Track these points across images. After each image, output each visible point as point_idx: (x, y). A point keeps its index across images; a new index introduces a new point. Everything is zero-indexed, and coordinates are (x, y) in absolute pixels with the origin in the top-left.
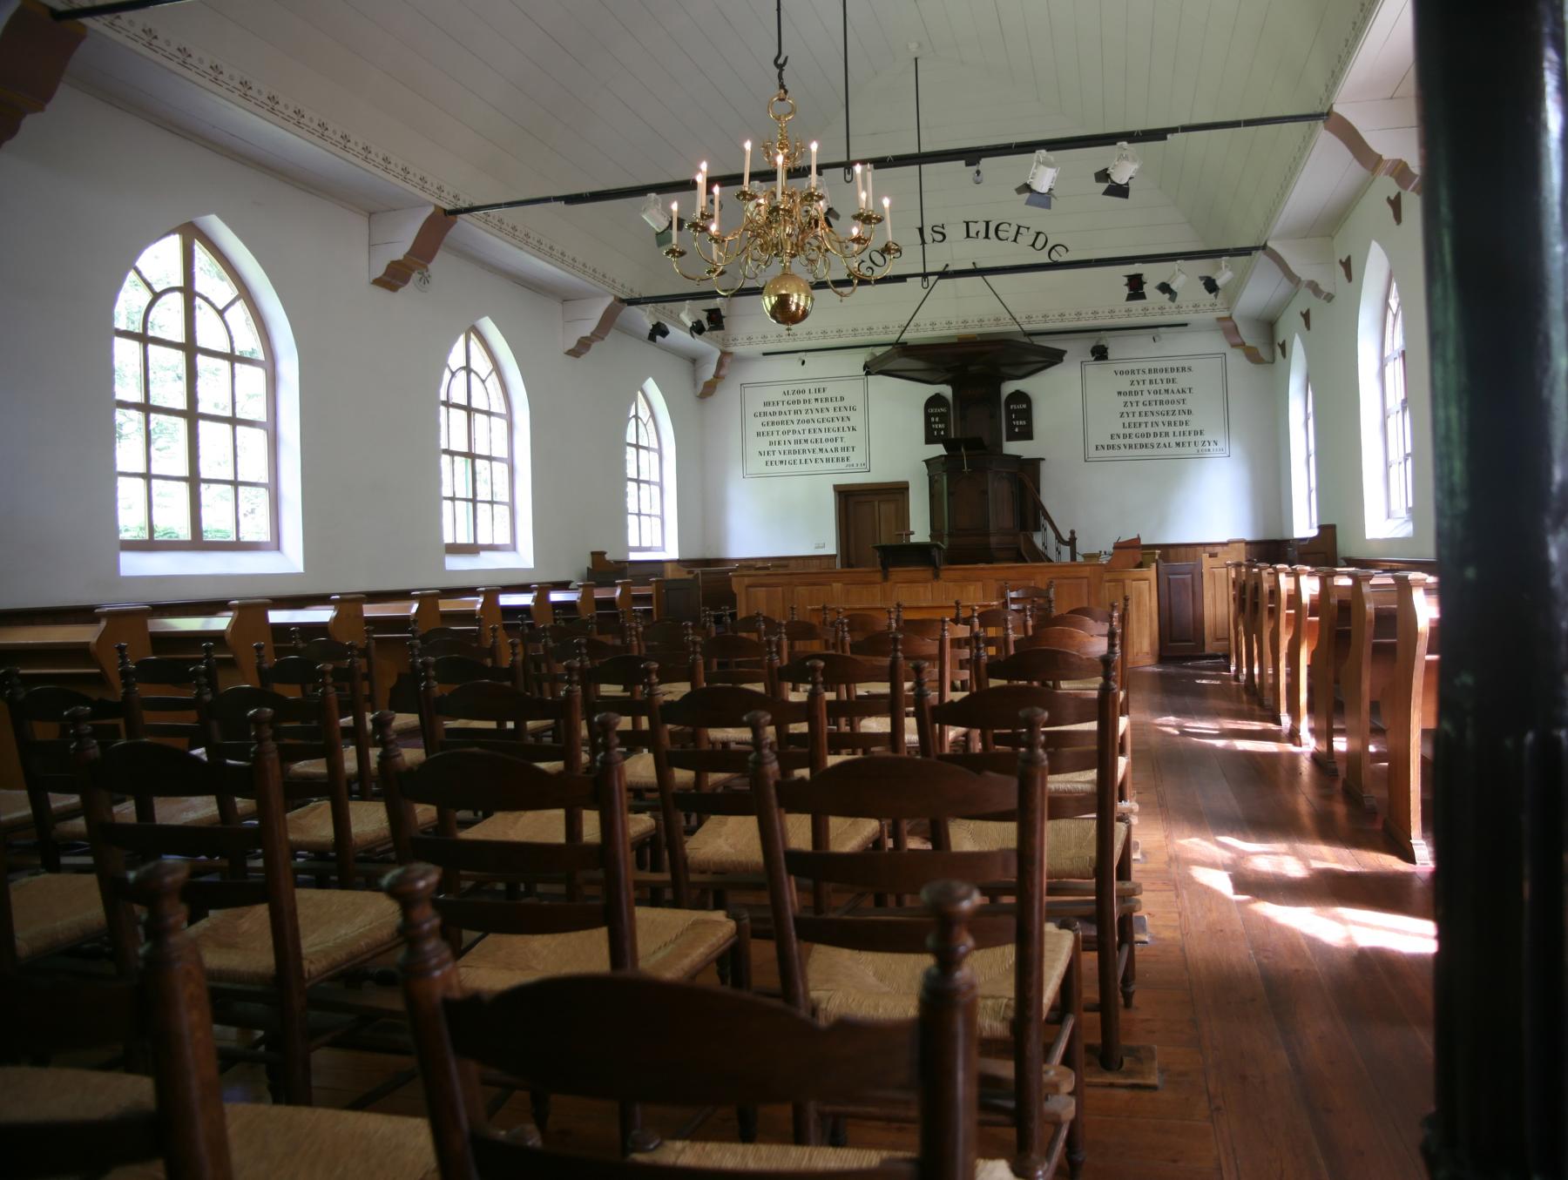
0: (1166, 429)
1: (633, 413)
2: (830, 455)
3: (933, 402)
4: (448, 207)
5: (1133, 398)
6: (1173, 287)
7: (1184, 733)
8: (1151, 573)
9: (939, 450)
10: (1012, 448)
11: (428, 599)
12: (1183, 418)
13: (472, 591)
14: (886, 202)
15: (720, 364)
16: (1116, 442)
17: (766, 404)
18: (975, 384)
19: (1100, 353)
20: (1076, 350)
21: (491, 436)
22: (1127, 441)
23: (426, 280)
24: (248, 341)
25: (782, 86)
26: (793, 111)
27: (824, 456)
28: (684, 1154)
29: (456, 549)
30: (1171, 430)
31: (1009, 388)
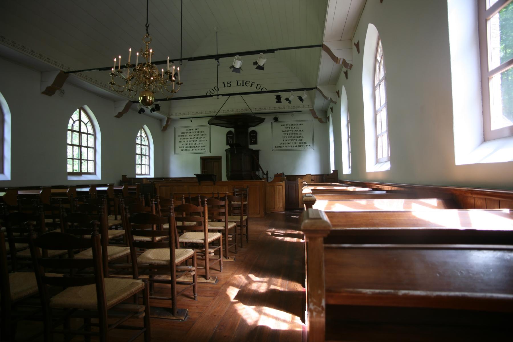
0: (296, 142)
1: (139, 134)
2: (199, 148)
3: (229, 133)
4: (65, 71)
5: (286, 133)
6: (290, 99)
7: (273, 234)
8: (283, 184)
9: (228, 147)
10: (251, 147)
11: (47, 189)
12: (301, 138)
13: (38, 188)
14: (178, 69)
15: (168, 121)
16: (281, 145)
17: (182, 133)
18: (241, 129)
19: (276, 120)
20: (269, 119)
22: (285, 145)
23: (63, 93)
24: (91, 131)
25: (147, 33)
26: (151, 40)
27: (198, 148)
29: (73, 174)
30: (297, 142)
31: (251, 129)
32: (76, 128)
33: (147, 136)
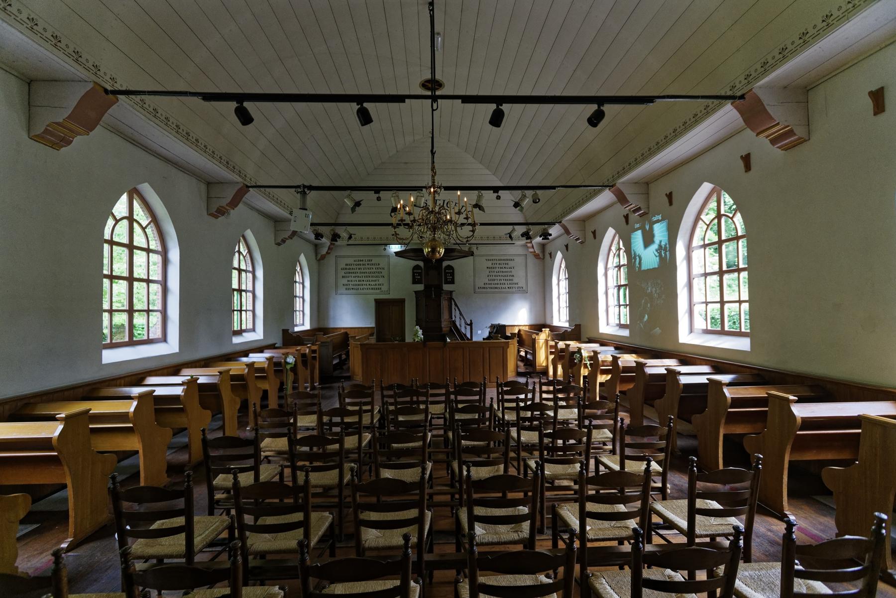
1: (237, 249)
3: (416, 267)
10: (446, 287)
21: (247, 284)
24: (155, 245)
28: (339, 589)
32: (120, 268)
33: (250, 252)
